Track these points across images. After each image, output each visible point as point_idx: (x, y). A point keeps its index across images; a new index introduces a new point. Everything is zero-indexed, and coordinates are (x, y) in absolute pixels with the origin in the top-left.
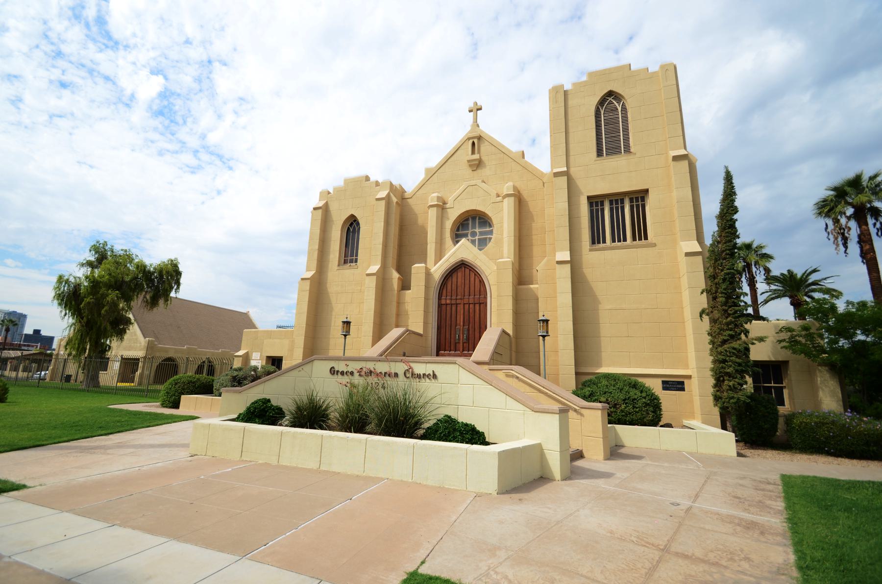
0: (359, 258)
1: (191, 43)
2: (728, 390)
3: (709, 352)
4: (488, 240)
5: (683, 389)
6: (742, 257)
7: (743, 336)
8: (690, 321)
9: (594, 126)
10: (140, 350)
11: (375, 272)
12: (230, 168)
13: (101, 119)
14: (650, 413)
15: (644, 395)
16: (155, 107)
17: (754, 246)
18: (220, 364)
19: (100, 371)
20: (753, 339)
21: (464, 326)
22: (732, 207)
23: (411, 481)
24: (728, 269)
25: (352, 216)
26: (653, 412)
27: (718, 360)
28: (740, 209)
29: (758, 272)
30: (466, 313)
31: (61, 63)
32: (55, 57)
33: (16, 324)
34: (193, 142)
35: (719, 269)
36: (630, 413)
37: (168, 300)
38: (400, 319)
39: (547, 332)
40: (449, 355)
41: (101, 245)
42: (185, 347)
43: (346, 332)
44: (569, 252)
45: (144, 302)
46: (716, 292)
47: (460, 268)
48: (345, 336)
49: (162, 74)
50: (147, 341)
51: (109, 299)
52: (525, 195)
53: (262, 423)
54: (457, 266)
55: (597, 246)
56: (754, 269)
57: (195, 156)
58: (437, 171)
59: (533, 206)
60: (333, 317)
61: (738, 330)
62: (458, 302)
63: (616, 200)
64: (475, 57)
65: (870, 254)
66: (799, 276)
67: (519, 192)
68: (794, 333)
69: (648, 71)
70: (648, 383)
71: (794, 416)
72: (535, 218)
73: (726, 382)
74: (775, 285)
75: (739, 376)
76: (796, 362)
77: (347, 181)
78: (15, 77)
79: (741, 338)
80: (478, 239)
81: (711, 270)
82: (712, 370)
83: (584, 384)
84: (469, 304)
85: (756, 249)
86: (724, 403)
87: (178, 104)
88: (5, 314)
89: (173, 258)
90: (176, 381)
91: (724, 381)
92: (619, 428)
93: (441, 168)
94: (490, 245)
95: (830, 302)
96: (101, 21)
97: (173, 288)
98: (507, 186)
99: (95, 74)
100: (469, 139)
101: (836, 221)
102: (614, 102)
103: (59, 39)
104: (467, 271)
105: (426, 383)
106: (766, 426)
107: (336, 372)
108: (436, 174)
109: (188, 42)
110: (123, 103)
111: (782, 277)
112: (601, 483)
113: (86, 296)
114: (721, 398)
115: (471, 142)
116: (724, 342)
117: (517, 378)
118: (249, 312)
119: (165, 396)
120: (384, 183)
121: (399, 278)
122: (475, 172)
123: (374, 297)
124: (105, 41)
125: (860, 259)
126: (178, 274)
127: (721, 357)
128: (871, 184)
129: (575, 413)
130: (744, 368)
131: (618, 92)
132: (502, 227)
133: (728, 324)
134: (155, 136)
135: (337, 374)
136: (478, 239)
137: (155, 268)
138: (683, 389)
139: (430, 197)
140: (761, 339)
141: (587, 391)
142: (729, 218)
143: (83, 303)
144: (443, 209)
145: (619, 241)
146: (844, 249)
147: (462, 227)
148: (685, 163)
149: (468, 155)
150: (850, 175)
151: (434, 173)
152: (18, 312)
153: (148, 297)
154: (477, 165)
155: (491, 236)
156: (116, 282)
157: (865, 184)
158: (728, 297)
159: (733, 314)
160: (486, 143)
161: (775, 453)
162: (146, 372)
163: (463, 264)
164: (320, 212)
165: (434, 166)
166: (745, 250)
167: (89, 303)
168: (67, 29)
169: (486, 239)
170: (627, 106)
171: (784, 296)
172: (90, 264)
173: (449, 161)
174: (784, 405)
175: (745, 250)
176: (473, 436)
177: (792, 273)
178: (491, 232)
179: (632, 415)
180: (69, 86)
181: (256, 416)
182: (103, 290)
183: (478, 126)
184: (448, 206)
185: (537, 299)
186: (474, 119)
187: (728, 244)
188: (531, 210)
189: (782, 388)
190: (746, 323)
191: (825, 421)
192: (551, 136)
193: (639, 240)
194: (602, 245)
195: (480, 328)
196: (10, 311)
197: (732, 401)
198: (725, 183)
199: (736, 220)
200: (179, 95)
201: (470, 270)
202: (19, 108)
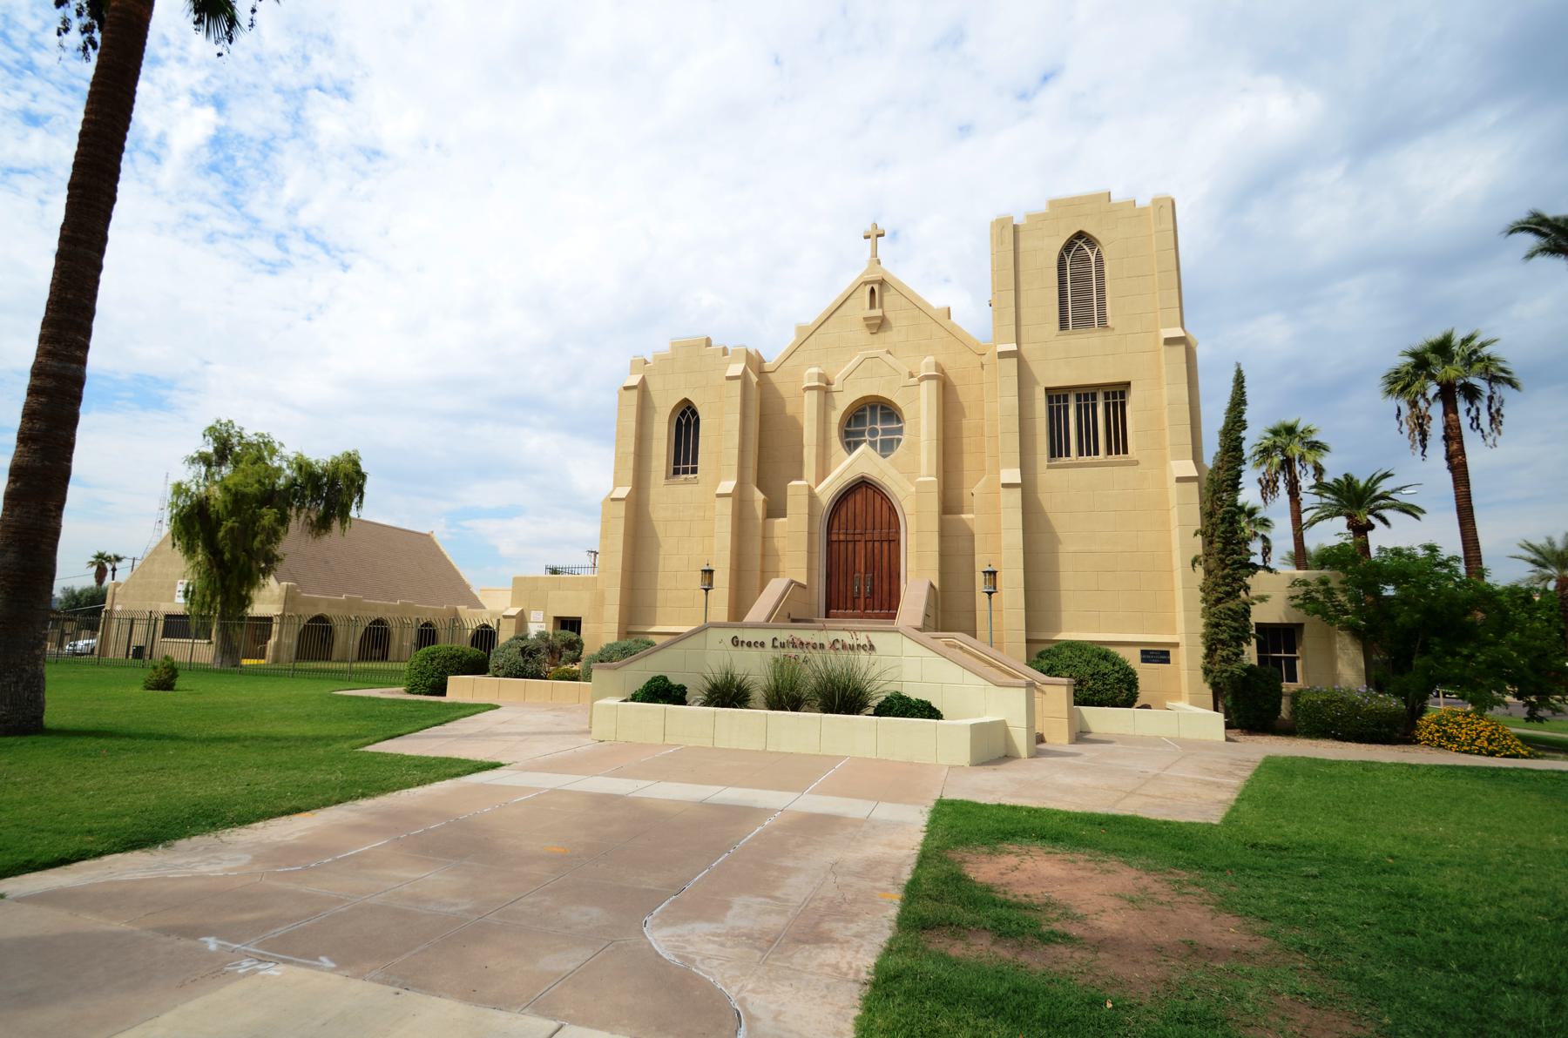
0: (700, 466)
2: (1220, 661)
3: (1201, 612)
5: (1168, 661)
6: (1279, 447)
7: (1242, 593)
8: (1180, 570)
9: (1057, 302)
10: (273, 602)
15: (1117, 668)
18: (399, 626)
20: (1253, 598)
22: (1240, 421)
24: (1228, 506)
25: (686, 400)
26: (1127, 690)
27: (1210, 624)
28: (1249, 424)
29: (1304, 472)
30: (869, 555)
35: (1217, 505)
36: (1099, 692)
37: (346, 522)
39: (995, 588)
40: (845, 616)
42: (344, 597)
44: (1019, 470)
46: (1212, 535)
48: (707, 590)
50: (285, 587)
52: (952, 374)
53: (668, 703)
56: (1298, 468)
59: (966, 393)
60: (661, 557)
61: (1236, 586)
62: (856, 539)
63: (1086, 395)
66: (1362, 484)
67: (943, 371)
68: (1310, 587)
69: (1135, 205)
70: (1122, 653)
71: (1300, 693)
72: (967, 411)
73: (1219, 652)
75: (1234, 644)
76: (1313, 627)
79: (1239, 596)
80: (881, 440)
81: (1208, 505)
82: (1203, 636)
83: (1041, 655)
84: (874, 541)
85: (1302, 435)
86: (1215, 678)
90: (433, 656)
91: (1216, 649)
92: (1084, 709)
93: (822, 327)
94: (899, 451)
98: (926, 363)
100: (866, 283)
101: (1413, 404)
102: (1085, 247)
104: (870, 492)
106: (1266, 706)
108: (813, 336)
111: (1335, 484)
112: (1070, 760)
114: (1212, 671)
115: (868, 288)
116: (1219, 601)
117: (961, 648)
118: (432, 532)
119: (417, 677)
121: (764, 501)
122: (875, 336)
123: (730, 529)
127: (1214, 620)
128: (1463, 350)
133: (1224, 578)
135: (742, 645)
136: (881, 440)
138: (1168, 661)
139: (808, 372)
140: (1262, 599)
141: (1045, 664)
142: (1233, 437)
144: (826, 392)
145: (1089, 454)
146: (1421, 449)
148: (1181, 349)
149: (864, 309)
150: (1436, 335)
151: (811, 335)
155: (900, 437)
157: (1456, 348)
158: (1227, 542)
159: (1232, 565)
160: (893, 291)
161: (1273, 738)
162: (286, 641)
163: (864, 482)
164: (634, 393)
165: (811, 323)
166: (1284, 436)
167: (232, 529)
169: (892, 440)
171: (1338, 514)
172: (204, 459)
173: (834, 316)
174: (1296, 681)
175: (1284, 436)
176: (927, 711)
177: (1352, 479)
178: (900, 431)
183: (879, 262)
184: (834, 388)
185: (973, 536)
186: (872, 251)
187: (1230, 473)
188: (961, 399)
189: (1295, 659)
190: (1247, 577)
193: (1116, 454)
194: (1064, 459)
197: (1224, 675)
198: (1234, 387)
199: (1244, 439)
201: (874, 491)
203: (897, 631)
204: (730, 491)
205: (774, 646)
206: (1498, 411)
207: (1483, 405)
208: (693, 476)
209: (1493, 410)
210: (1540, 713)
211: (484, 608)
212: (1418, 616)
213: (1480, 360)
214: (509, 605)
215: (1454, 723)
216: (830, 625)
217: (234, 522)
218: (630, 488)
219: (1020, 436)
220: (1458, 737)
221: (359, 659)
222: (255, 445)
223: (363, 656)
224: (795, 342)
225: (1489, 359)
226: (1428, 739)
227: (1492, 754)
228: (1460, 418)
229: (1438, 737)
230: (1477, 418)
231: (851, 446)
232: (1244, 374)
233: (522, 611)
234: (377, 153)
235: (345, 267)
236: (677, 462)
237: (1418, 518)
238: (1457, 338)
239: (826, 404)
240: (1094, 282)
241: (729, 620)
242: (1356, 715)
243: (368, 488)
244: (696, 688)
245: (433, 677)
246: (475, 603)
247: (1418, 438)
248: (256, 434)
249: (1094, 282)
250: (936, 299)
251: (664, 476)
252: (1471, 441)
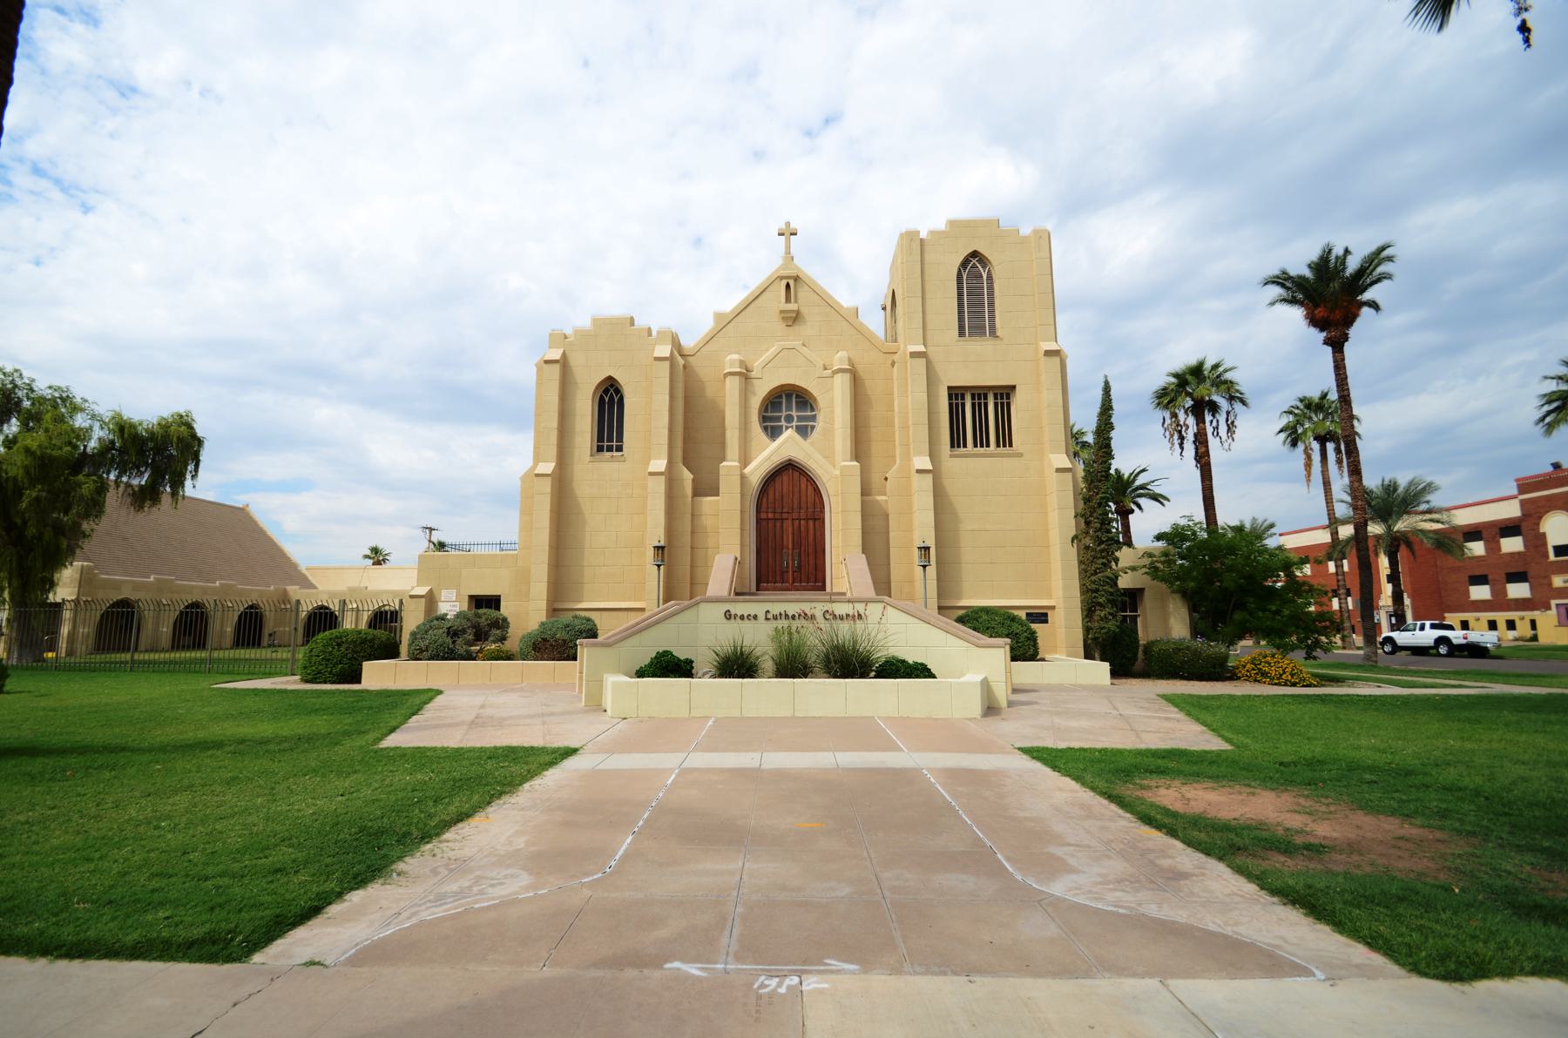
4: (809, 428)
5: (1046, 622)
21: (793, 549)
25: (610, 378)
42: (152, 579)
50: (80, 567)
53: (679, 677)
59: (873, 387)
63: (979, 394)
75: (1110, 605)
89: (182, 411)
91: (1095, 610)
93: (740, 316)
94: (815, 435)
100: (782, 278)
101: (1174, 415)
102: (978, 265)
107: (733, 617)
115: (784, 283)
118: (247, 506)
121: (693, 480)
125: (1194, 462)
133: (1102, 551)
138: (1046, 622)
145: (982, 446)
147: (772, 407)
149: (780, 302)
150: (1192, 361)
155: (814, 424)
159: (1107, 541)
160: (806, 287)
162: (83, 630)
164: (557, 367)
167: (37, 499)
169: (806, 426)
170: (994, 276)
178: (813, 418)
184: (753, 374)
185: (888, 515)
189: (1136, 617)
190: (1117, 551)
195: (816, 552)
204: (549, 471)
205: (767, 619)
206: (1233, 422)
207: (1222, 418)
208: (620, 454)
209: (1229, 422)
210: (1314, 654)
211: (316, 588)
212: (1242, 581)
213: (1226, 382)
214: (415, 585)
215: (1266, 662)
216: (836, 597)
217: (40, 491)
218: (554, 464)
219: (929, 428)
221: (173, 647)
222: (49, 400)
223: (176, 645)
224: (713, 329)
225: (1231, 382)
226: (1247, 676)
227: (1294, 685)
230: (1217, 428)
231: (773, 433)
232: (1111, 384)
233: (431, 591)
234: (133, 90)
235: (87, 209)
236: (600, 439)
237: (1163, 505)
238: (1208, 365)
239: (746, 389)
240: (986, 296)
243: (205, 456)
244: (704, 660)
245: (340, 664)
246: (305, 583)
247: (1177, 442)
248: (50, 387)
249: (986, 296)
252: (1213, 443)
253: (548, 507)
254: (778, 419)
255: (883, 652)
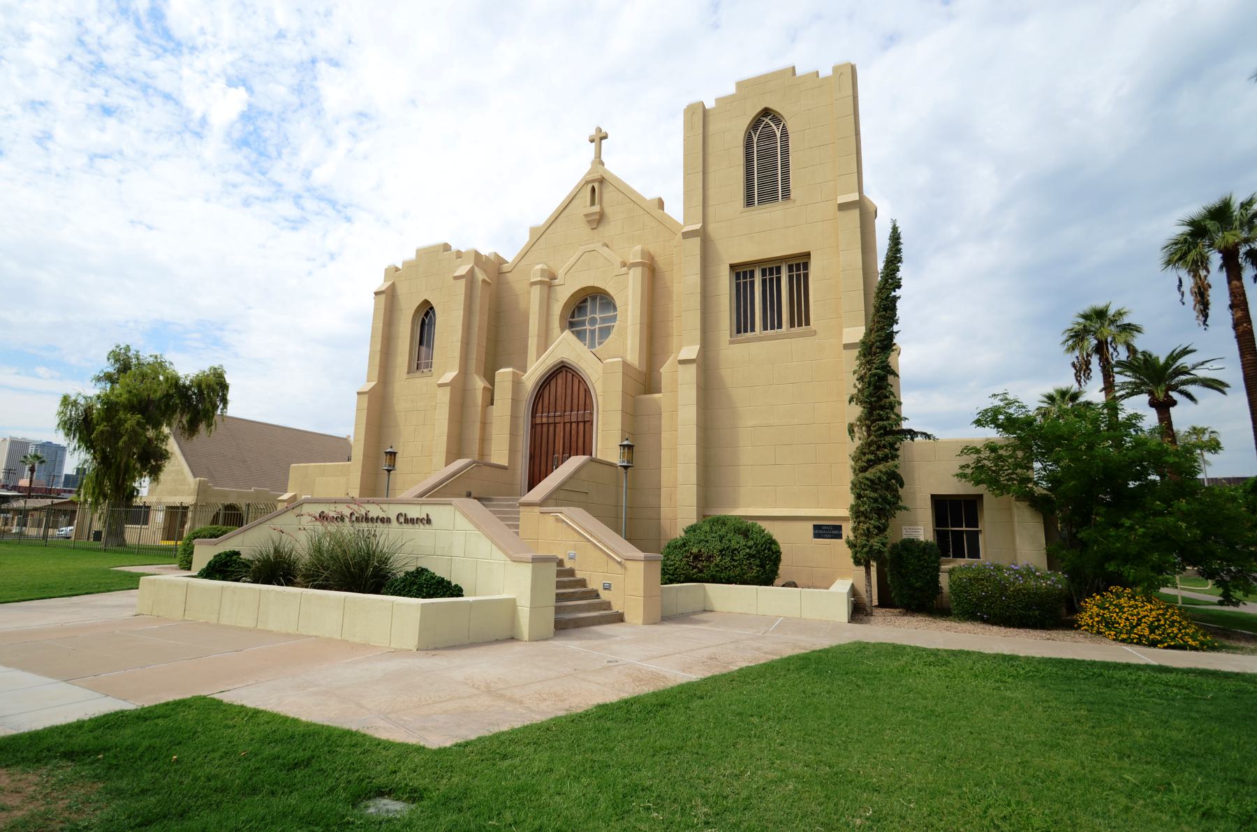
1: (284, 36)
10: (190, 495)
11: (448, 381)
12: (348, 219)
13: (161, 157)
14: (754, 568)
16: (236, 135)
17: (1111, 312)
19: (126, 524)
21: (563, 453)
23: (339, 638)
24: (876, 369)
25: (426, 302)
31: (104, 80)
32: (94, 71)
33: (43, 462)
34: (293, 183)
36: (726, 568)
37: (212, 425)
38: (580, 442)
39: (394, 466)
41: (123, 351)
43: (389, 466)
45: (180, 428)
47: (560, 372)
48: (389, 471)
49: (244, 85)
51: (128, 425)
52: (661, 262)
54: (557, 370)
55: (743, 336)
57: (297, 204)
58: (544, 232)
63: (770, 268)
64: (716, 26)
65: (1242, 325)
66: (1162, 360)
74: (1126, 375)
77: (421, 253)
78: (41, 104)
80: (599, 328)
87: (269, 128)
88: (36, 447)
95: (1005, 412)
96: (156, 15)
97: (218, 407)
99: (151, 91)
100: (587, 183)
102: (771, 124)
103: (100, 44)
105: (421, 529)
108: (543, 236)
109: (281, 35)
110: (191, 132)
113: (99, 423)
115: (590, 186)
120: (468, 253)
121: (485, 388)
122: (595, 231)
124: (163, 42)
126: (224, 387)
129: (619, 566)
130: (880, 506)
131: (773, 108)
132: (626, 310)
134: (237, 177)
136: (599, 328)
137: (192, 381)
143: (95, 432)
148: (855, 214)
150: (1213, 201)
152: (54, 443)
153: (184, 421)
154: (598, 220)
156: (140, 402)
160: (611, 188)
163: (564, 366)
164: (383, 297)
167: (102, 432)
168: (109, 30)
172: (109, 378)
174: (979, 557)
177: (1150, 356)
178: (614, 318)
179: (729, 570)
180: (115, 112)
181: (217, 572)
182: (121, 415)
183: (602, 164)
186: (596, 153)
189: (977, 533)
191: (980, 577)
192: (684, 177)
194: (749, 334)
196: (43, 441)
200: (270, 114)
202: (47, 149)
203: (451, 504)
220: (1118, 623)
224: (528, 243)
226: (1088, 625)
227: (1153, 644)
228: (1245, 285)
229: (1098, 622)
237: (1224, 393)
241: (360, 497)
242: (1001, 595)
250: (649, 192)
251: (406, 371)
253: (365, 422)
254: (583, 323)
255: (402, 565)
